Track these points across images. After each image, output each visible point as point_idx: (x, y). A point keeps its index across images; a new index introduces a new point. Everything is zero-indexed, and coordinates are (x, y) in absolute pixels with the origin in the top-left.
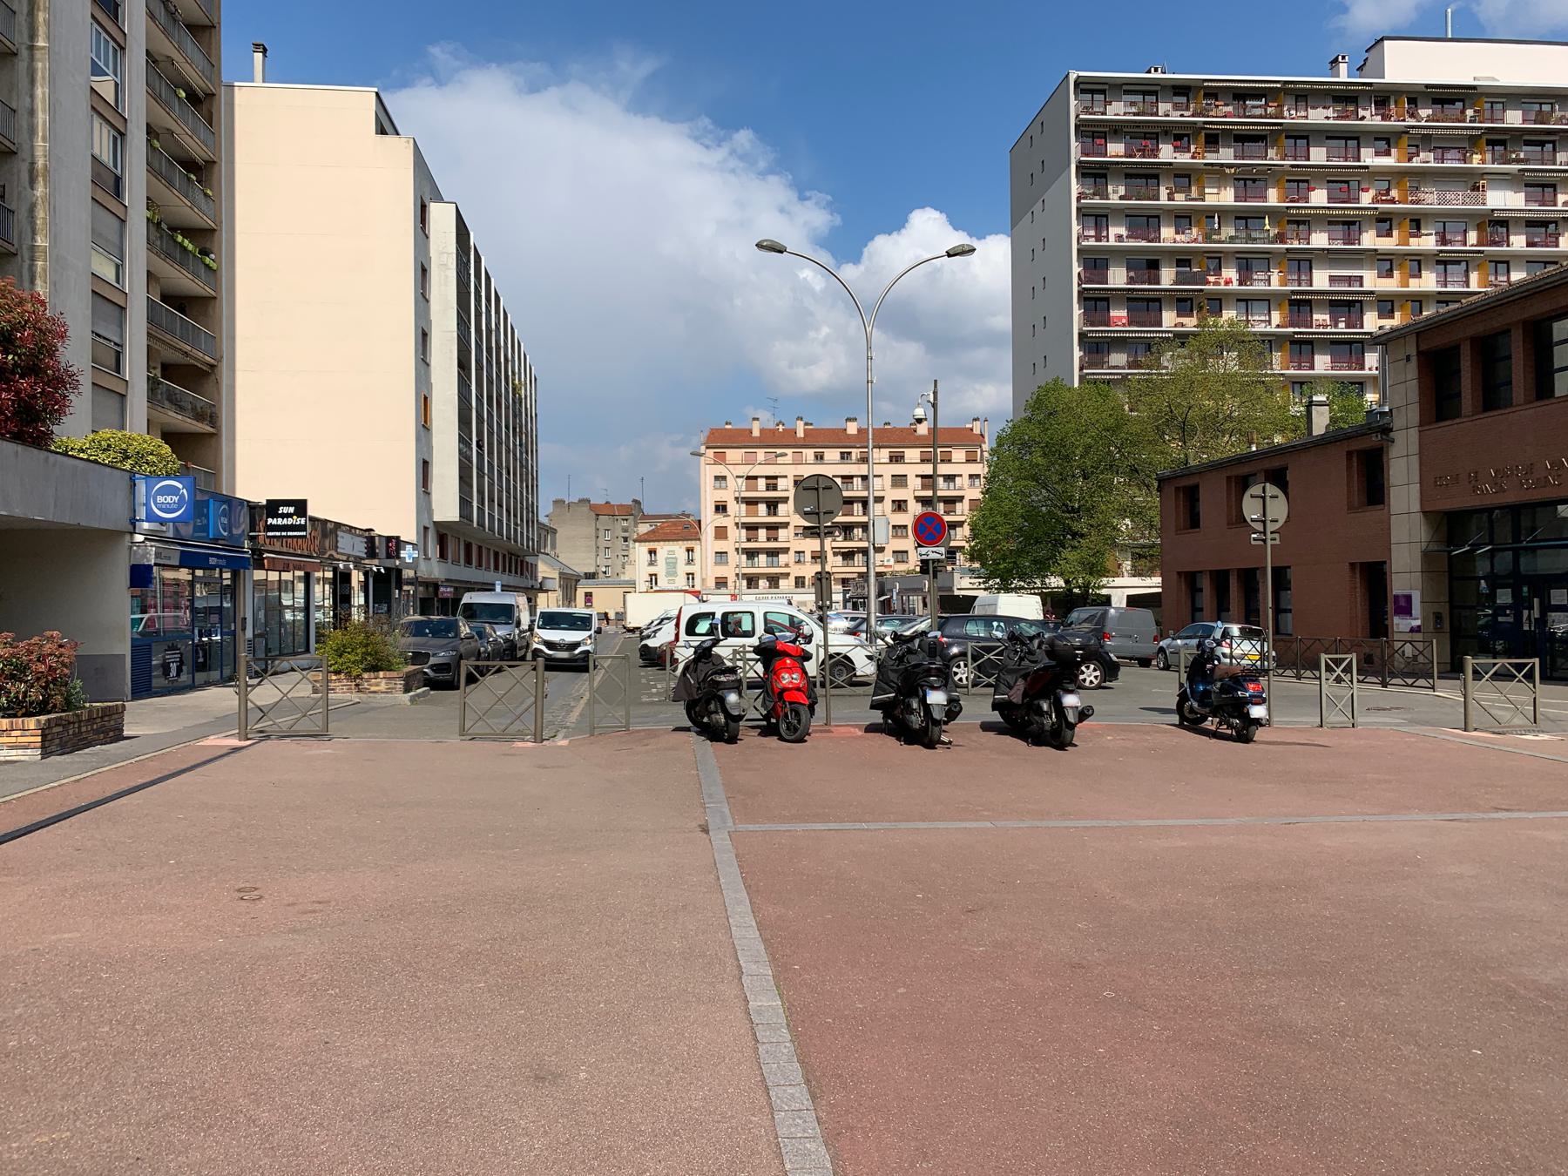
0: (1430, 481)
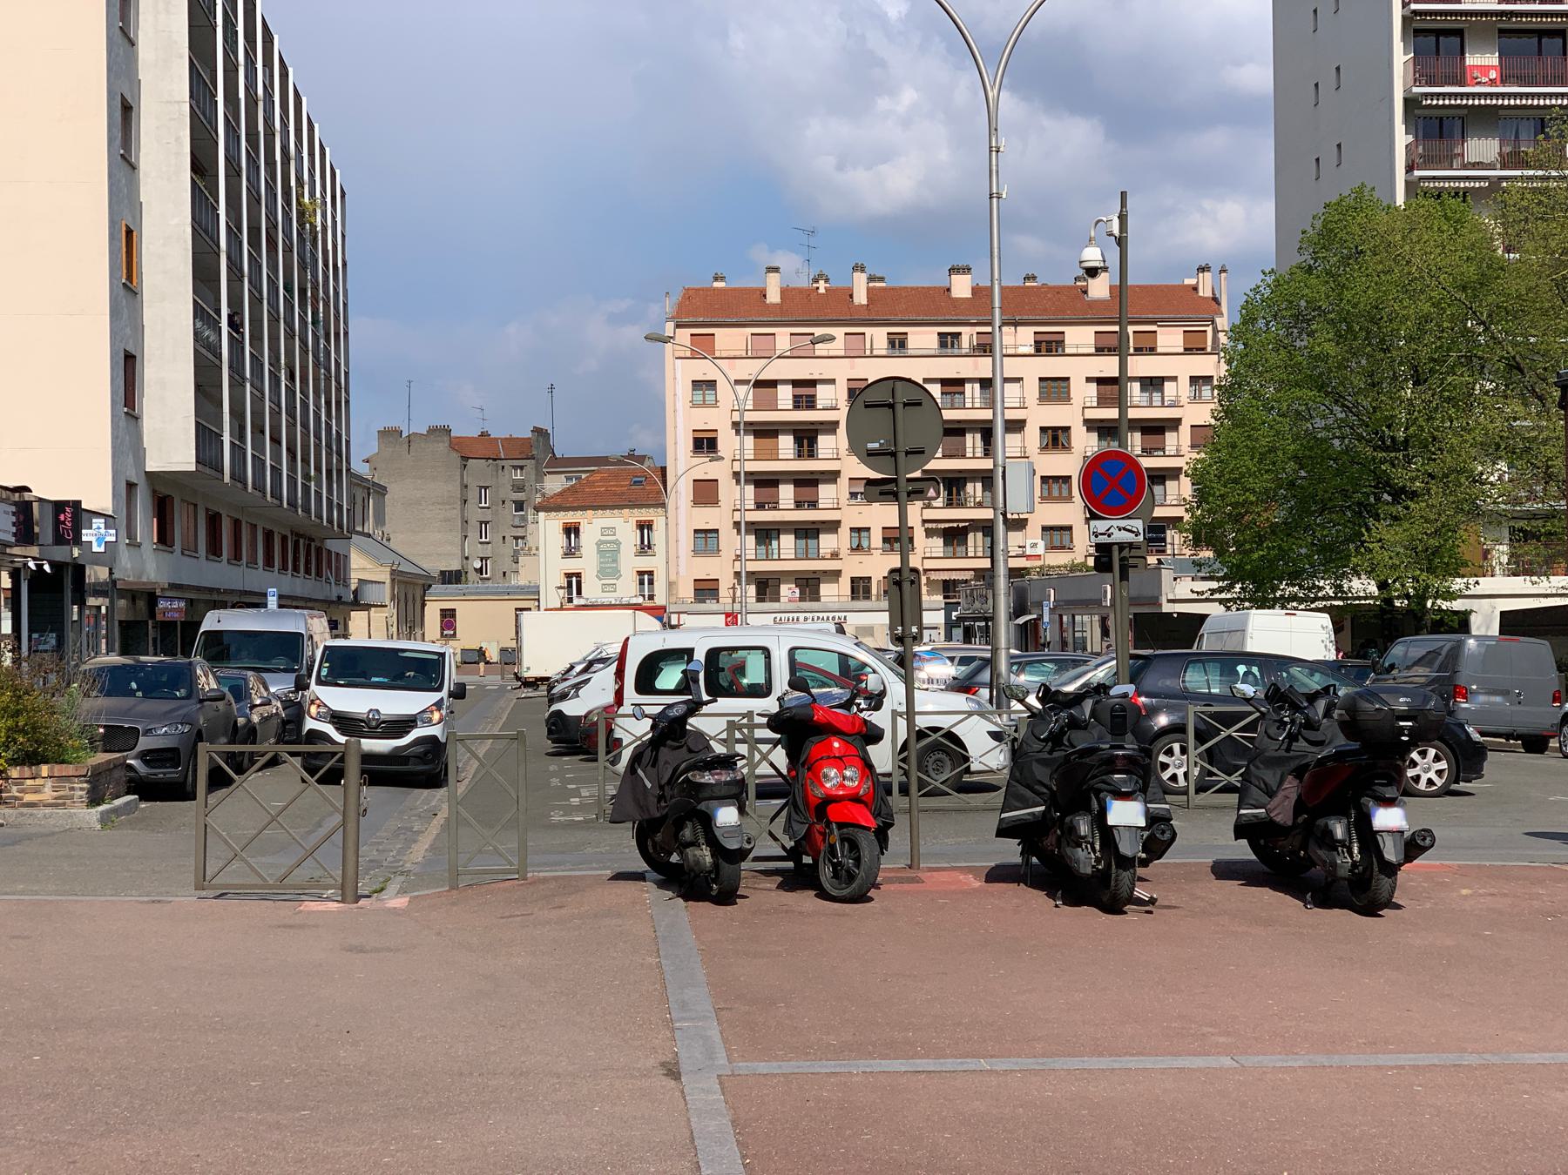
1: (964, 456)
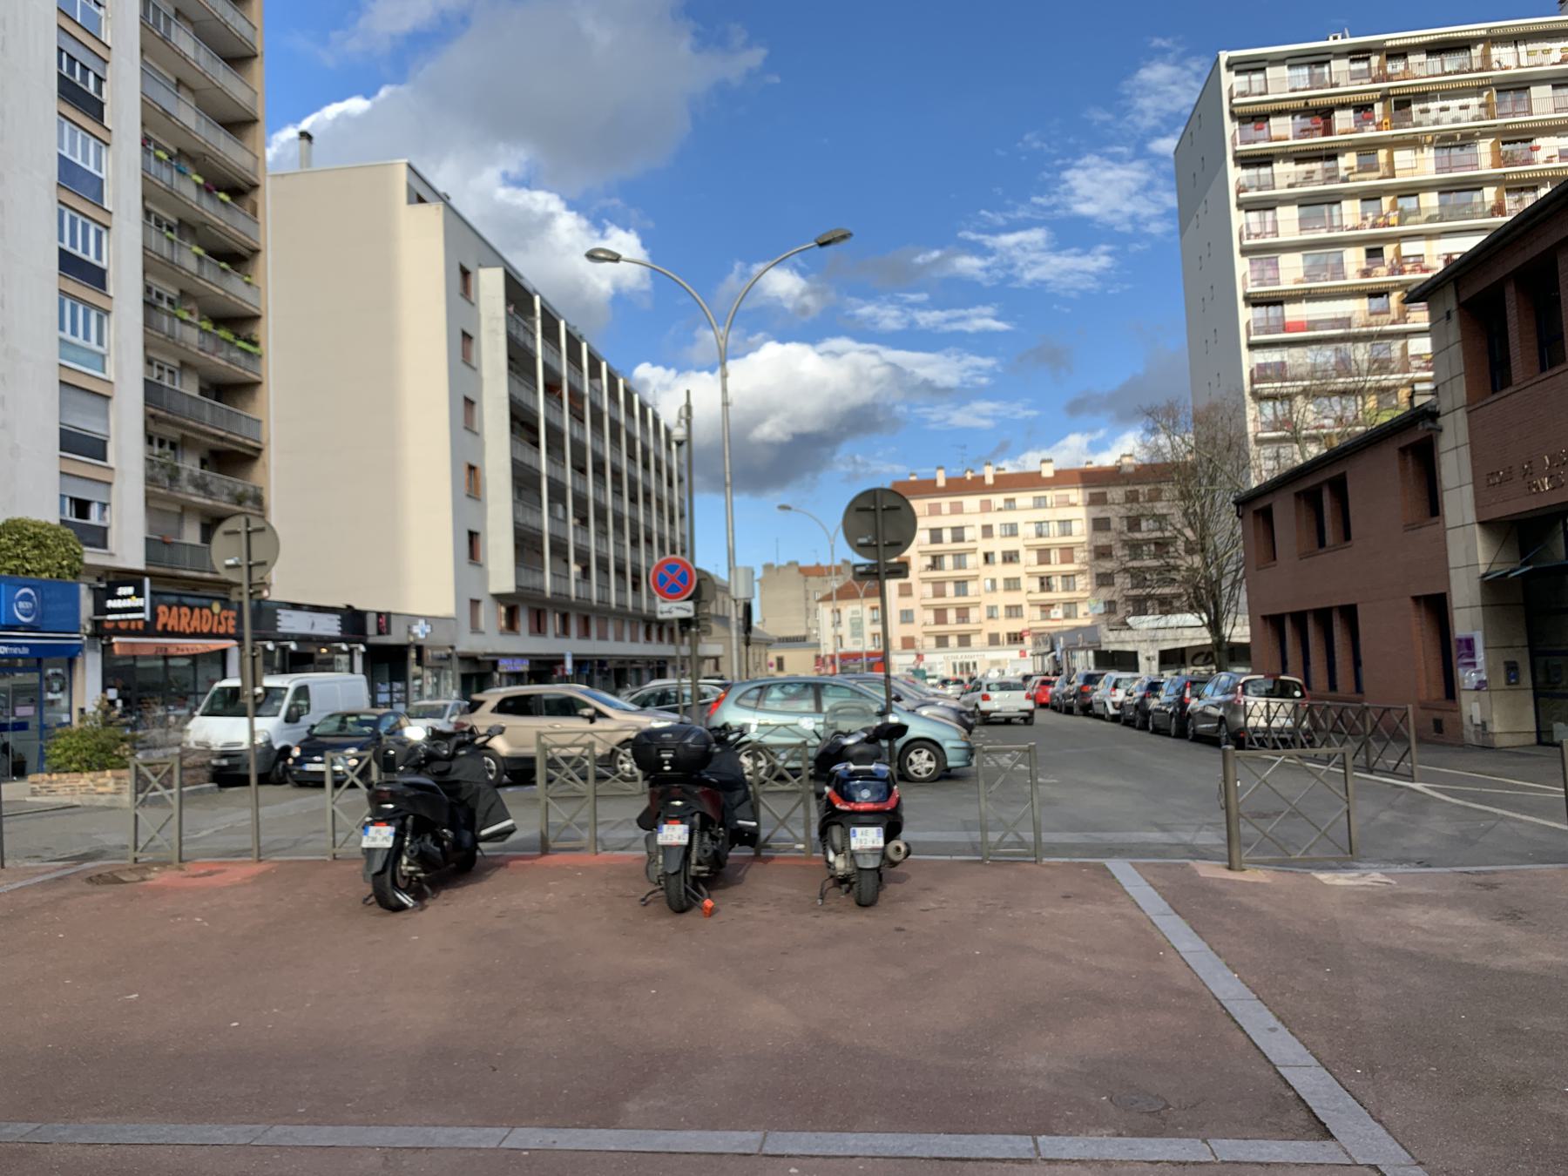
0: (1486, 481)
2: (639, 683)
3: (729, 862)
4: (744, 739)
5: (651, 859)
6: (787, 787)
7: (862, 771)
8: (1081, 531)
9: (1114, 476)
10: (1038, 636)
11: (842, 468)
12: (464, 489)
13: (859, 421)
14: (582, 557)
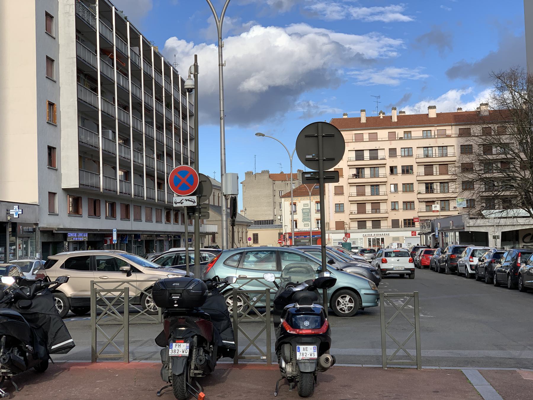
1: (432, 175)
2: (162, 250)
3: (216, 368)
4: (229, 287)
5: (165, 365)
6: (257, 319)
7: (305, 307)
8: (453, 153)
9: (475, 117)
10: (424, 221)
11: (300, 109)
12: (46, 119)
13: (313, 79)
14: (125, 166)
